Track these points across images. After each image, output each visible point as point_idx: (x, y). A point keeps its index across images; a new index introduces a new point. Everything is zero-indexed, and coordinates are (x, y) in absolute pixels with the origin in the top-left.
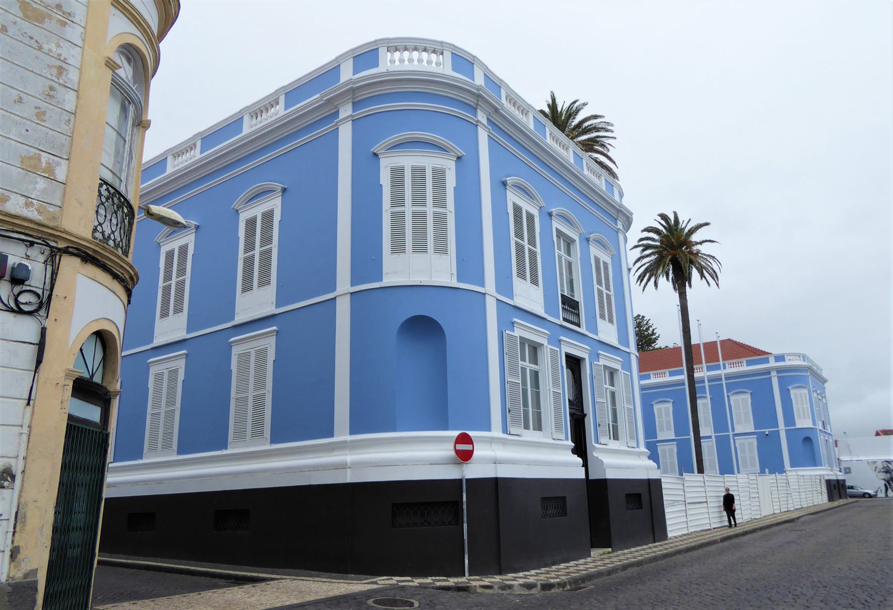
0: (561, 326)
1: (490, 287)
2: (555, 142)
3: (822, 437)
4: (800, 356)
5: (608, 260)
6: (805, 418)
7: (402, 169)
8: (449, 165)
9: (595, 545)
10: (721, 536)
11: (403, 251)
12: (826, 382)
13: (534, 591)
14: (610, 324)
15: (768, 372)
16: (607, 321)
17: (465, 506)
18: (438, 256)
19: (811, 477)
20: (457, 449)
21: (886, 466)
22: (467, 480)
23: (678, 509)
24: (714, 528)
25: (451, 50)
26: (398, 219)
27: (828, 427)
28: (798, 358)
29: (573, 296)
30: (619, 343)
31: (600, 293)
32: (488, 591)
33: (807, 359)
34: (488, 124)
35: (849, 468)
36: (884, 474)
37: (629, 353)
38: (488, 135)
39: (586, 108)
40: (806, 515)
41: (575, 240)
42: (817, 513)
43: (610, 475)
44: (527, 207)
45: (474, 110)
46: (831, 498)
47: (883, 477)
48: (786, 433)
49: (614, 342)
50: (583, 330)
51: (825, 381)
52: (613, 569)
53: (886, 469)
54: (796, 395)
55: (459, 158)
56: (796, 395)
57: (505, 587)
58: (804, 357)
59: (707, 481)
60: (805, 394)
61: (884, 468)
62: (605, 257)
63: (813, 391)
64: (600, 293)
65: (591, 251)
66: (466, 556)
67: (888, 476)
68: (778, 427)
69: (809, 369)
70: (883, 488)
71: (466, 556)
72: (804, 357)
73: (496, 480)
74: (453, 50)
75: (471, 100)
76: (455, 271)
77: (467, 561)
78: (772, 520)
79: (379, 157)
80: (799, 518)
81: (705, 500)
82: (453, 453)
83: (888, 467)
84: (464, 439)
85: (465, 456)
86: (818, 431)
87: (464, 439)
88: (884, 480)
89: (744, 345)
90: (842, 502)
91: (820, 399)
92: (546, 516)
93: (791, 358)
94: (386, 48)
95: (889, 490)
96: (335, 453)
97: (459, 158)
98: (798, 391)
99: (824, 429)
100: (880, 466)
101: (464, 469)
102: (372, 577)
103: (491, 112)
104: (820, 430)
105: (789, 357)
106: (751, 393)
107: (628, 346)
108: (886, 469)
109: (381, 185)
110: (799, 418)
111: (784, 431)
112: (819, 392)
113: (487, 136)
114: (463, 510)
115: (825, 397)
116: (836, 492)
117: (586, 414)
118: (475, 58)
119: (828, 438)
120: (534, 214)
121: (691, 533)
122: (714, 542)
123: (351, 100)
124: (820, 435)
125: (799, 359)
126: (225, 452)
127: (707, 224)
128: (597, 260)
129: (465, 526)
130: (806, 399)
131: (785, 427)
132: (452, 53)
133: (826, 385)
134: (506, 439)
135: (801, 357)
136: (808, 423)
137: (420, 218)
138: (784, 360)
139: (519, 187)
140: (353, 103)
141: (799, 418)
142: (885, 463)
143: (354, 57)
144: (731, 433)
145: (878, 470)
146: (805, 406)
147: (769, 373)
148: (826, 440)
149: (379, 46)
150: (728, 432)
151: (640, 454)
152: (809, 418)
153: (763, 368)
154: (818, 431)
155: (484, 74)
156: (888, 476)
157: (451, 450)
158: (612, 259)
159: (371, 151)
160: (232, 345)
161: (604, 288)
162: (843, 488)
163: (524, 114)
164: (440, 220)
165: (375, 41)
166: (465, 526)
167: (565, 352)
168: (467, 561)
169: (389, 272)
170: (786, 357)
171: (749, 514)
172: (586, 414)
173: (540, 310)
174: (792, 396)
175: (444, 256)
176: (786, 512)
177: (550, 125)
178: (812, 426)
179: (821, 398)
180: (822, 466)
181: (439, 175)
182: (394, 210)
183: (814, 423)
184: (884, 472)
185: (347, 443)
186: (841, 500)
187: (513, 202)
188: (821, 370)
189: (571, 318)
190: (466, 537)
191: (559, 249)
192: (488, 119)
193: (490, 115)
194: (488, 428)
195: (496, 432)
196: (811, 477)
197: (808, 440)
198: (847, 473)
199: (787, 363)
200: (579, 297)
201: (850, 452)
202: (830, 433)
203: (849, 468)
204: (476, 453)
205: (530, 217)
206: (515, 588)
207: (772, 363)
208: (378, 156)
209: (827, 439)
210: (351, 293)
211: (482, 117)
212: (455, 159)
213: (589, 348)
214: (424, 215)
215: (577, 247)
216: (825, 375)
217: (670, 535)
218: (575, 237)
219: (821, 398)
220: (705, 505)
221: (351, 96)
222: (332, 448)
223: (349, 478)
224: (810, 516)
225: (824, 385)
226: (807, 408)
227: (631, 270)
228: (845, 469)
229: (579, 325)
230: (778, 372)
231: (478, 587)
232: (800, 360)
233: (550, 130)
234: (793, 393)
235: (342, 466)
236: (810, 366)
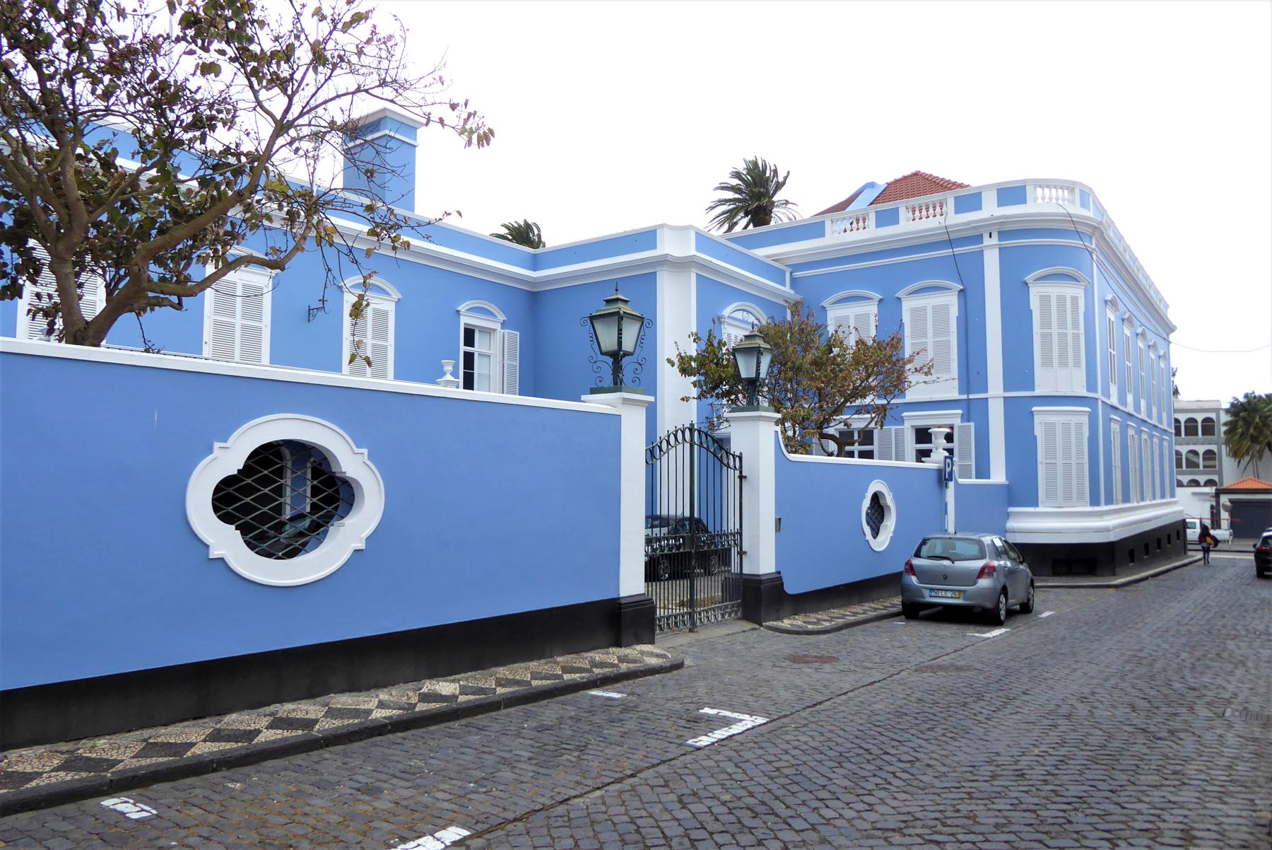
4: (1072, 190)
6: (1064, 364)
11: (1051, 364)
12: (1173, 331)
26: (1047, 338)
51: (1171, 329)
54: (1045, 300)
72: (1086, 195)
98: (1054, 290)
102: (986, 629)
106: (881, 301)
110: (1047, 363)
126: (1038, 510)
128: (1109, 319)
131: (1005, 390)
133: (1172, 337)
135: (1077, 192)
137: (1063, 337)
140: (999, 232)
147: (979, 239)
153: (964, 224)
160: (658, 513)
165: (1023, 181)
174: (1035, 304)
181: (1075, 300)
188: (1167, 306)
216: (1173, 316)
230: (1003, 235)
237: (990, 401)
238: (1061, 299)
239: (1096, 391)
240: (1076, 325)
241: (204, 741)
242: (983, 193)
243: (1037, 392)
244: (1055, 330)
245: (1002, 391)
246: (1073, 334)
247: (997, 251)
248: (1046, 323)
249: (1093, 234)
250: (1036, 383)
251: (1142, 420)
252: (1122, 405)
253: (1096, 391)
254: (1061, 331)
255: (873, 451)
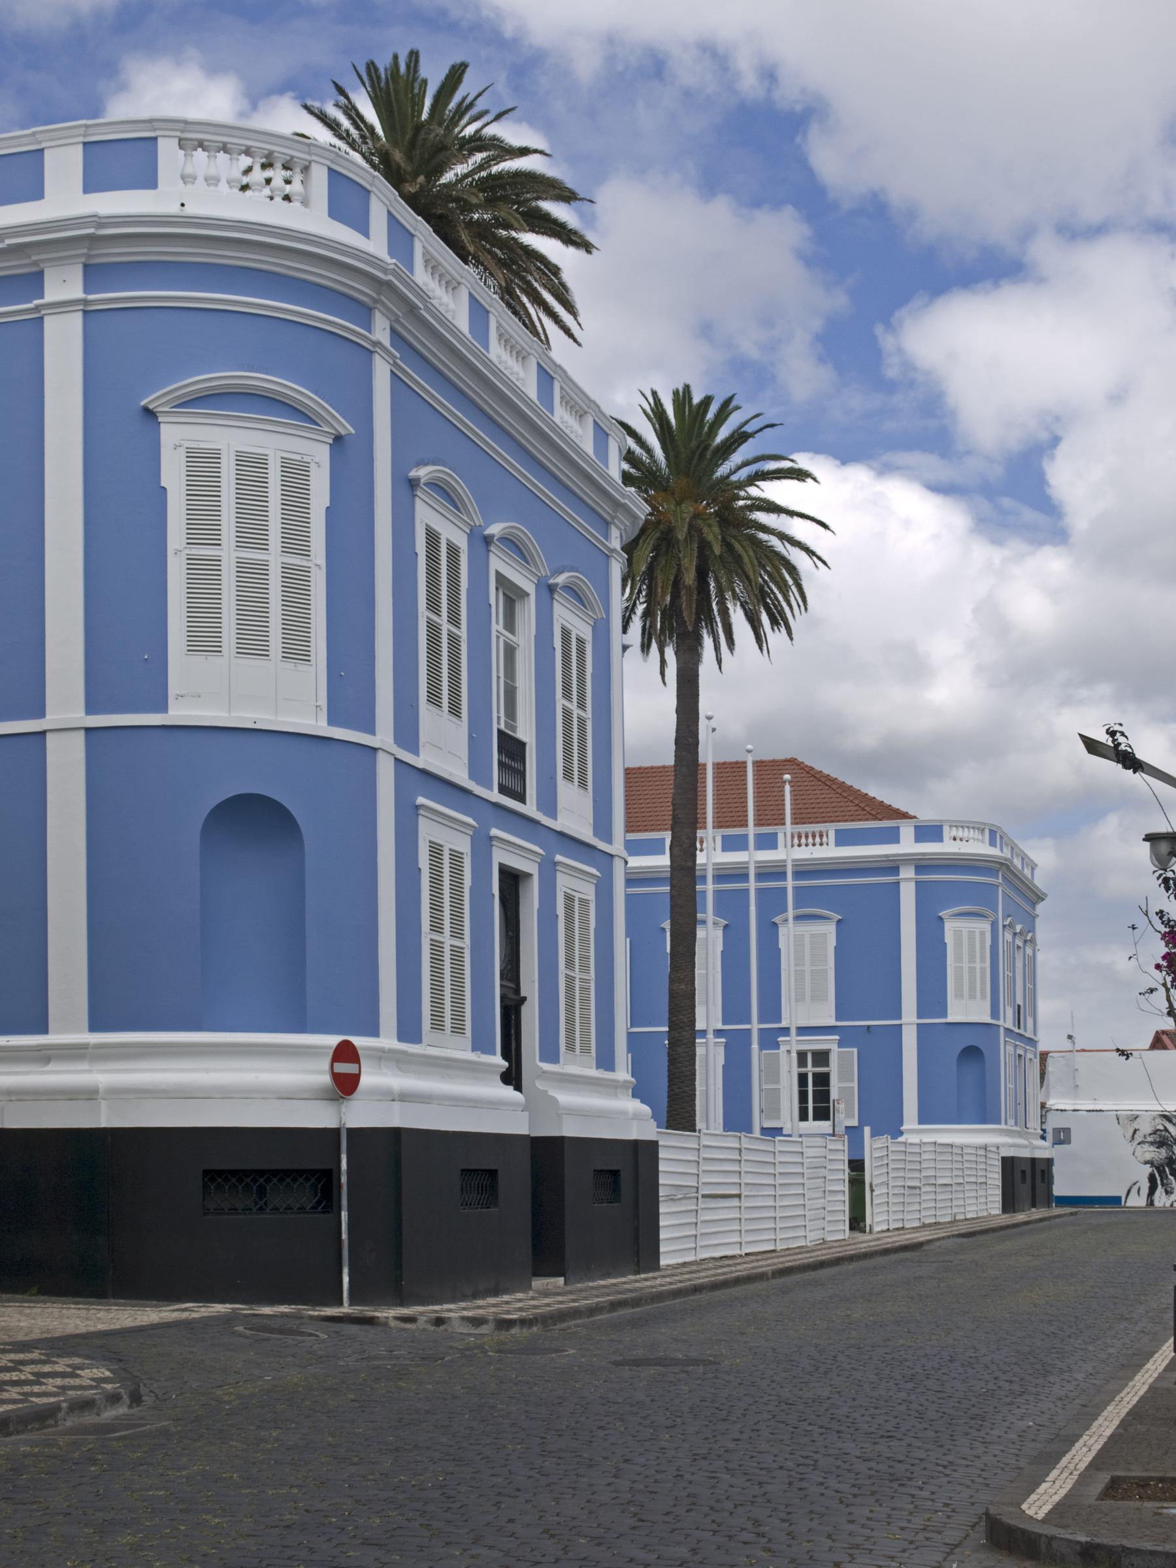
0: (497, 806)
1: (383, 736)
2: (503, 346)
3: (1010, 1048)
5: (587, 633)
6: (972, 996)
7: (214, 456)
8: (319, 455)
9: (538, 1273)
10: (775, 1267)
13: (485, 1329)
14: (581, 791)
15: (891, 867)
16: (576, 783)
17: (344, 1179)
18: (289, 665)
19: (998, 1148)
20: (335, 1071)
21: (1162, 1128)
22: (351, 1131)
23: (683, 1209)
24: (746, 1254)
25: (328, 163)
27: (1030, 1021)
28: (977, 835)
29: (514, 729)
30: (595, 834)
31: (567, 713)
32: (408, 1326)
33: (1001, 838)
34: (392, 345)
35: (1067, 1131)
36: (1152, 1148)
37: (612, 856)
38: (392, 371)
39: (580, 254)
40: (949, 1237)
41: (528, 595)
42: (975, 1234)
43: (571, 1129)
44: (453, 533)
45: (363, 313)
46: (1009, 1203)
47: (1148, 1157)
48: (917, 1027)
49: (585, 833)
50: (530, 808)
52: (597, 1305)
53: (1160, 1136)
55: (338, 439)
56: (958, 934)
57: (439, 1321)
58: (993, 833)
59: (745, 1148)
60: (982, 933)
61: (1155, 1132)
62: (582, 629)
63: (1004, 926)
64: (567, 713)
65: (555, 616)
66: (346, 1271)
67: (1163, 1153)
68: (900, 1018)
69: (1003, 866)
70: (1145, 1186)
71: (346, 1271)
73: (396, 1133)
74: (332, 161)
75: (362, 290)
76: (323, 702)
77: (346, 1279)
78: (873, 1244)
79: (160, 420)
80: (929, 1242)
81: (737, 1192)
82: (326, 1079)
83: (1166, 1130)
84: (346, 1052)
85: (346, 1085)
86: (1002, 1031)
87: (346, 1052)
88: (1150, 1163)
89: (834, 780)
90: (1036, 1214)
91: (1019, 947)
92: (476, 1206)
93: (960, 833)
94: (177, 140)
95: (1160, 1190)
96: (51, 1067)
97: (338, 439)
98: (965, 925)
99: (1019, 1028)
100: (1145, 1127)
101: (343, 1110)
103: (400, 315)
104: (1007, 1030)
105: (954, 832)
106: (839, 921)
107: (609, 839)
108: (1160, 1136)
109: (164, 488)
110: (959, 995)
111: (915, 1027)
112: (1018, 928)
113: (389, 374)
114: (340, 1186)
115: (1033, 941)
116: (1024, 1190)
117: (525, 999)
118: (1144, 910)
119: (1026, 1051)
120: (440, 531)
121: (700, 1260)
122: (761, 1277)
123: (83, 260)
124: (1005, 1042)
125: (980, 837)
127: (830, 568)
129: (344, 1215)
130: (983, 947)
131: (919, 1017)
132: (330, 169)
133: (1040, 908)
134: (405, 1053)
136: (979, 1013)
137: (253, 574)
138: (939, 839)
139: (439, 488)
140: (86, 267)
141: (959, 995)
142: (1158, 1121)
143: (85, 144)
144: (755, 1026)
145: (1139, 1138)
146: (978, 965)
147: (895, 870)
148: (1020, 1056)
149: (158, 133)
150: (749, 1022)
151: (614, 1087)
152: (983, 997)
154: (1002, 1031)
155: (389, 213)
156: (1163, 1153)
157: (321, 1072)
158: (594, 628)
159: (143, 403)
161: (575, 704)
162: (1043, 1180)
163: (450, 289)
164: (295, 581)
166: (344, 1215)
167: (500, 864)
168: (346, 1279)
169: (183, 692)
170: (946, 829)
171: (820, 1229)
172: (525, 999)
173: (459, 774)
174: (949, 938)
175: (302, 667)
176: (898, 1229)
177: (500, 309)
178: (988, 1020)
179: (1021, 944)
180: (999, 1123)
181: (295, 473)
182: (193, 552)
183: (995, 1013)
184: (1152, 1143)
185: (87, 1048)
186: (1034, 1210)
187: (427, 525)
189: (511, 783)
190: (344, 1236)
191: (497, 623)
192: (393, 330)
193: (397, 320)
194: (374, 1032)
195: (388, 1040)
196: (998, 1148)
197: (971, 1054)
198: (1060, 1142)
199: (946, 847)
200: (525, 731)
201: (1075, 1090)
202: (1032, 1036)
203: (1067, 1131)
204: (366, 1080)
205: (453, 551)
206: (456, 1324)
207: (907, 845)
208: (157, 418)
209: (1022, 1053)
210: (88, 730)
211: (381, 332)
212: (331, 441)
213: (541, 851)
214: (262, 569)
215: (527, 614)
217: (664, 1261)
218: (529, 587)
219: (1021, 944)
220: (735, 1202)
221: (85, 251)
222: (44, 1056)
223: (105, 1118)
224: (960, 1240)
225: (1034, 909)
226: (983, 970)
227: (628, 650)
228: (1057, 1131)
229: (521, 798)
230: (919, 869)
231: (391, 1318)
232: (983, 841)
233: (497, 322)
234: (952, 929)
235: (89, 1094)
236: (1006, 859)
237: (903, 1026)
238: (971, 934)
239: (998, 1019)
240: (983, 959)
241: (30, 1373)
242: (49, 157)
243: (951, 1018)
244: (229, 554)
245: (81, 713)
246: (974, 962)
247: (913, 885)
248: (959, 958)
249: (1000, 869)
250: (173, 689)
251: (1028, 1038)
252: (601, 839)
253: (998, 1019)
254: (974, 965)
255: (839, 1082)
